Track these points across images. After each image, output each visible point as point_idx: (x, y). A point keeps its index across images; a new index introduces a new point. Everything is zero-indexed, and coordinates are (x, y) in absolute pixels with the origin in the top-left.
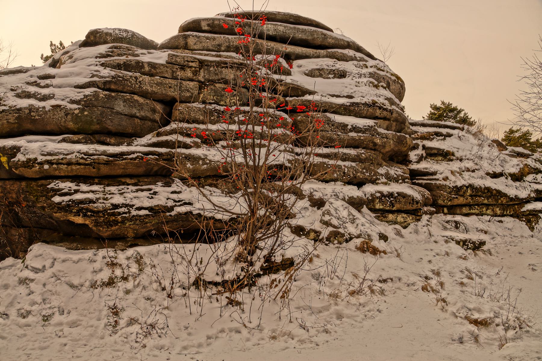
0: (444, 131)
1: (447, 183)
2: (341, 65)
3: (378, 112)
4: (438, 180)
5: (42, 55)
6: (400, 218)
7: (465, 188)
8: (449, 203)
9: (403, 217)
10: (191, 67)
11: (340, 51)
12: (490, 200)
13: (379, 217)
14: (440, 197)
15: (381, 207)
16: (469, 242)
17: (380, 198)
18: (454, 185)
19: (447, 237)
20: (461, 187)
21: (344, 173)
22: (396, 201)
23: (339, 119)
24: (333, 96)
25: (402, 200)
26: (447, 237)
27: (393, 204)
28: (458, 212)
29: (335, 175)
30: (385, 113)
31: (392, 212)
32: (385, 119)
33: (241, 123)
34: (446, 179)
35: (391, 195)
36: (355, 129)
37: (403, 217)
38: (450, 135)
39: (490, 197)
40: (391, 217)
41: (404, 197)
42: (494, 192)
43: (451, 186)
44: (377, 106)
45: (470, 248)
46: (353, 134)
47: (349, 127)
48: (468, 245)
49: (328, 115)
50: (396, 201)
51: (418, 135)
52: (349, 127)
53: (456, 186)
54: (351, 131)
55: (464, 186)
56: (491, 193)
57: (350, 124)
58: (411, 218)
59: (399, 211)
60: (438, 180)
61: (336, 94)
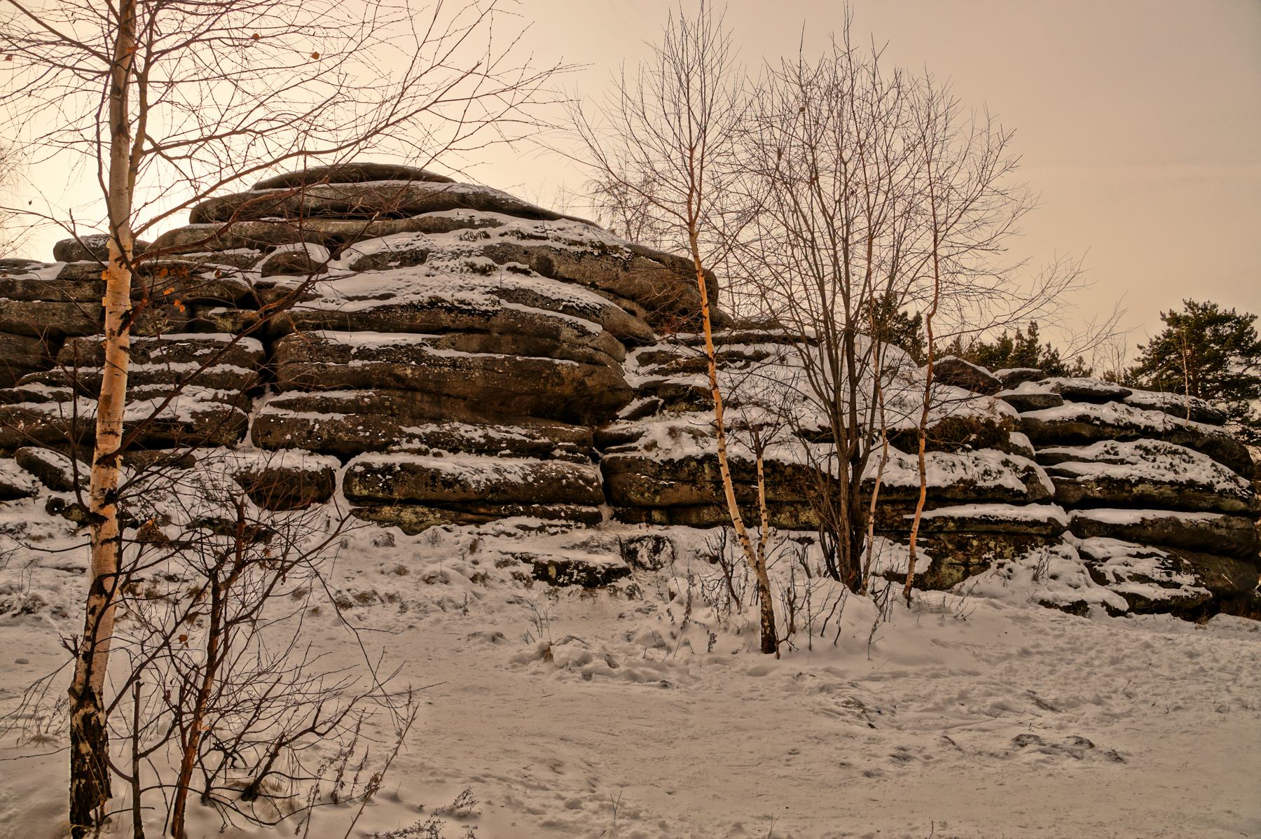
0: (749, 350)
1: (651, 455)
2: (422, 242)
3: (445, 319)
4: (635, 449)
5: (1163, 316)
6: (408, 515)
7: (694, 464)
8: (658, 499)
9: (416, 513)
10: (91, 280)
11: (435, 214)
12: (780, 491)
13: (360, 511)
14: (631, 485)
15: (365, 492)
16: (576, 567)
17: (362, 476)
18: (666, 458)
19: (513, 555)
20: (681, 461)
21: (310, 432)
22: (396, 481)
23: (342, 338)
24: (350, 299)
25: (407, 476)
26: (513, 555)
27: (389, 487)
28: (694, 519)
29: (288, 437)
30: (465, 318)
31: (390, 502)
32: (469, 330)
33: (158, 360)
34: (652, 446)
35: (388, 469)
36: (364, 353)
37: (416, 513)
38: (759, 357)
39: (780, 483)
40: (387, 511)
41: (413, 473)
42: (789, 470)
43: (657, 460)
44: (442, 307)
45: (577, 582)
46: (357, 363)
47: (353, 351)
48: (571, 575)
49: (319, 333)
50: (396, 481)
51: (677, 363)
52: (353, 351)
53: (671, 460)
54: (355, 357)
55: (690, 458)
56: (782, 473)
57: (356, 346)
58: (438, 515)
59: (409, 502)
60: (635, 449)
61: (360, 295)
